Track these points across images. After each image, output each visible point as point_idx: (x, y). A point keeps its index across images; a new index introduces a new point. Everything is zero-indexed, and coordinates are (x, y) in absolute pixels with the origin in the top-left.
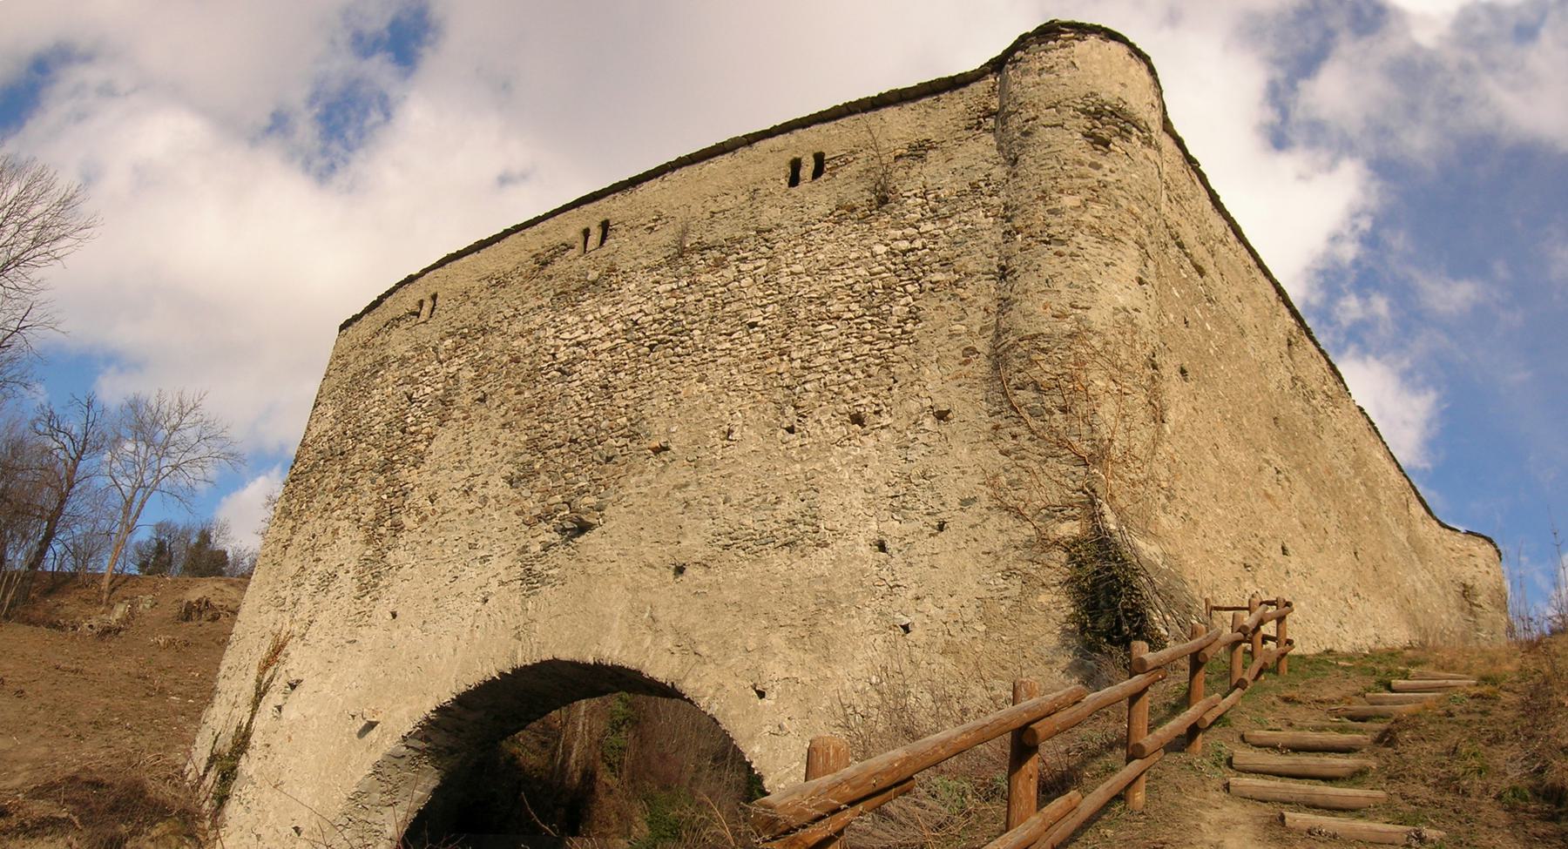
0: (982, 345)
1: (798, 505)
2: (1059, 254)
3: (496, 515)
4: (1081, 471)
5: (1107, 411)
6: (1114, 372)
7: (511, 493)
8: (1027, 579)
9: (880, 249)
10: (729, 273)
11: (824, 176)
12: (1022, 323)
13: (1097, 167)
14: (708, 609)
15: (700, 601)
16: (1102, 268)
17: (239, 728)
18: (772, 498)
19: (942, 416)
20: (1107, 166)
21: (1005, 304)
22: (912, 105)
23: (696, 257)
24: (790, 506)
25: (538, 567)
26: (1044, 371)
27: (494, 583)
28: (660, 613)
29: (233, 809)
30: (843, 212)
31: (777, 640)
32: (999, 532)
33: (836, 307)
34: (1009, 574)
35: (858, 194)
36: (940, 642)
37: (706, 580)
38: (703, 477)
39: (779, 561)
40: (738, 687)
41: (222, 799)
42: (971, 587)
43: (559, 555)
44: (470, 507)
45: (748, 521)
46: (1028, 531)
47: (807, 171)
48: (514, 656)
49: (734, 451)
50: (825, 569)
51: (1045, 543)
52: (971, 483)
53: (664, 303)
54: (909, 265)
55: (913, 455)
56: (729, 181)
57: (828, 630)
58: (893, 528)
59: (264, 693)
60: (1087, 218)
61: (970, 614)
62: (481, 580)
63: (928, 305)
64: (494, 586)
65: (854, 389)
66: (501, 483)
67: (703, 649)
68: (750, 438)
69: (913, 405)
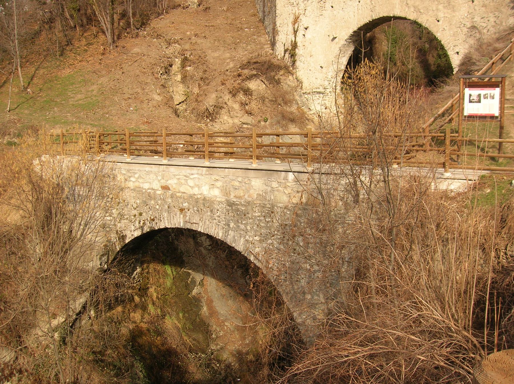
17: (292, 41)
29: (298, 63)
31: (441, 7)
36: (481, 3)
40: (432, 20)
41: (294, 62)
57: (453, 4)
67: (422, 11)
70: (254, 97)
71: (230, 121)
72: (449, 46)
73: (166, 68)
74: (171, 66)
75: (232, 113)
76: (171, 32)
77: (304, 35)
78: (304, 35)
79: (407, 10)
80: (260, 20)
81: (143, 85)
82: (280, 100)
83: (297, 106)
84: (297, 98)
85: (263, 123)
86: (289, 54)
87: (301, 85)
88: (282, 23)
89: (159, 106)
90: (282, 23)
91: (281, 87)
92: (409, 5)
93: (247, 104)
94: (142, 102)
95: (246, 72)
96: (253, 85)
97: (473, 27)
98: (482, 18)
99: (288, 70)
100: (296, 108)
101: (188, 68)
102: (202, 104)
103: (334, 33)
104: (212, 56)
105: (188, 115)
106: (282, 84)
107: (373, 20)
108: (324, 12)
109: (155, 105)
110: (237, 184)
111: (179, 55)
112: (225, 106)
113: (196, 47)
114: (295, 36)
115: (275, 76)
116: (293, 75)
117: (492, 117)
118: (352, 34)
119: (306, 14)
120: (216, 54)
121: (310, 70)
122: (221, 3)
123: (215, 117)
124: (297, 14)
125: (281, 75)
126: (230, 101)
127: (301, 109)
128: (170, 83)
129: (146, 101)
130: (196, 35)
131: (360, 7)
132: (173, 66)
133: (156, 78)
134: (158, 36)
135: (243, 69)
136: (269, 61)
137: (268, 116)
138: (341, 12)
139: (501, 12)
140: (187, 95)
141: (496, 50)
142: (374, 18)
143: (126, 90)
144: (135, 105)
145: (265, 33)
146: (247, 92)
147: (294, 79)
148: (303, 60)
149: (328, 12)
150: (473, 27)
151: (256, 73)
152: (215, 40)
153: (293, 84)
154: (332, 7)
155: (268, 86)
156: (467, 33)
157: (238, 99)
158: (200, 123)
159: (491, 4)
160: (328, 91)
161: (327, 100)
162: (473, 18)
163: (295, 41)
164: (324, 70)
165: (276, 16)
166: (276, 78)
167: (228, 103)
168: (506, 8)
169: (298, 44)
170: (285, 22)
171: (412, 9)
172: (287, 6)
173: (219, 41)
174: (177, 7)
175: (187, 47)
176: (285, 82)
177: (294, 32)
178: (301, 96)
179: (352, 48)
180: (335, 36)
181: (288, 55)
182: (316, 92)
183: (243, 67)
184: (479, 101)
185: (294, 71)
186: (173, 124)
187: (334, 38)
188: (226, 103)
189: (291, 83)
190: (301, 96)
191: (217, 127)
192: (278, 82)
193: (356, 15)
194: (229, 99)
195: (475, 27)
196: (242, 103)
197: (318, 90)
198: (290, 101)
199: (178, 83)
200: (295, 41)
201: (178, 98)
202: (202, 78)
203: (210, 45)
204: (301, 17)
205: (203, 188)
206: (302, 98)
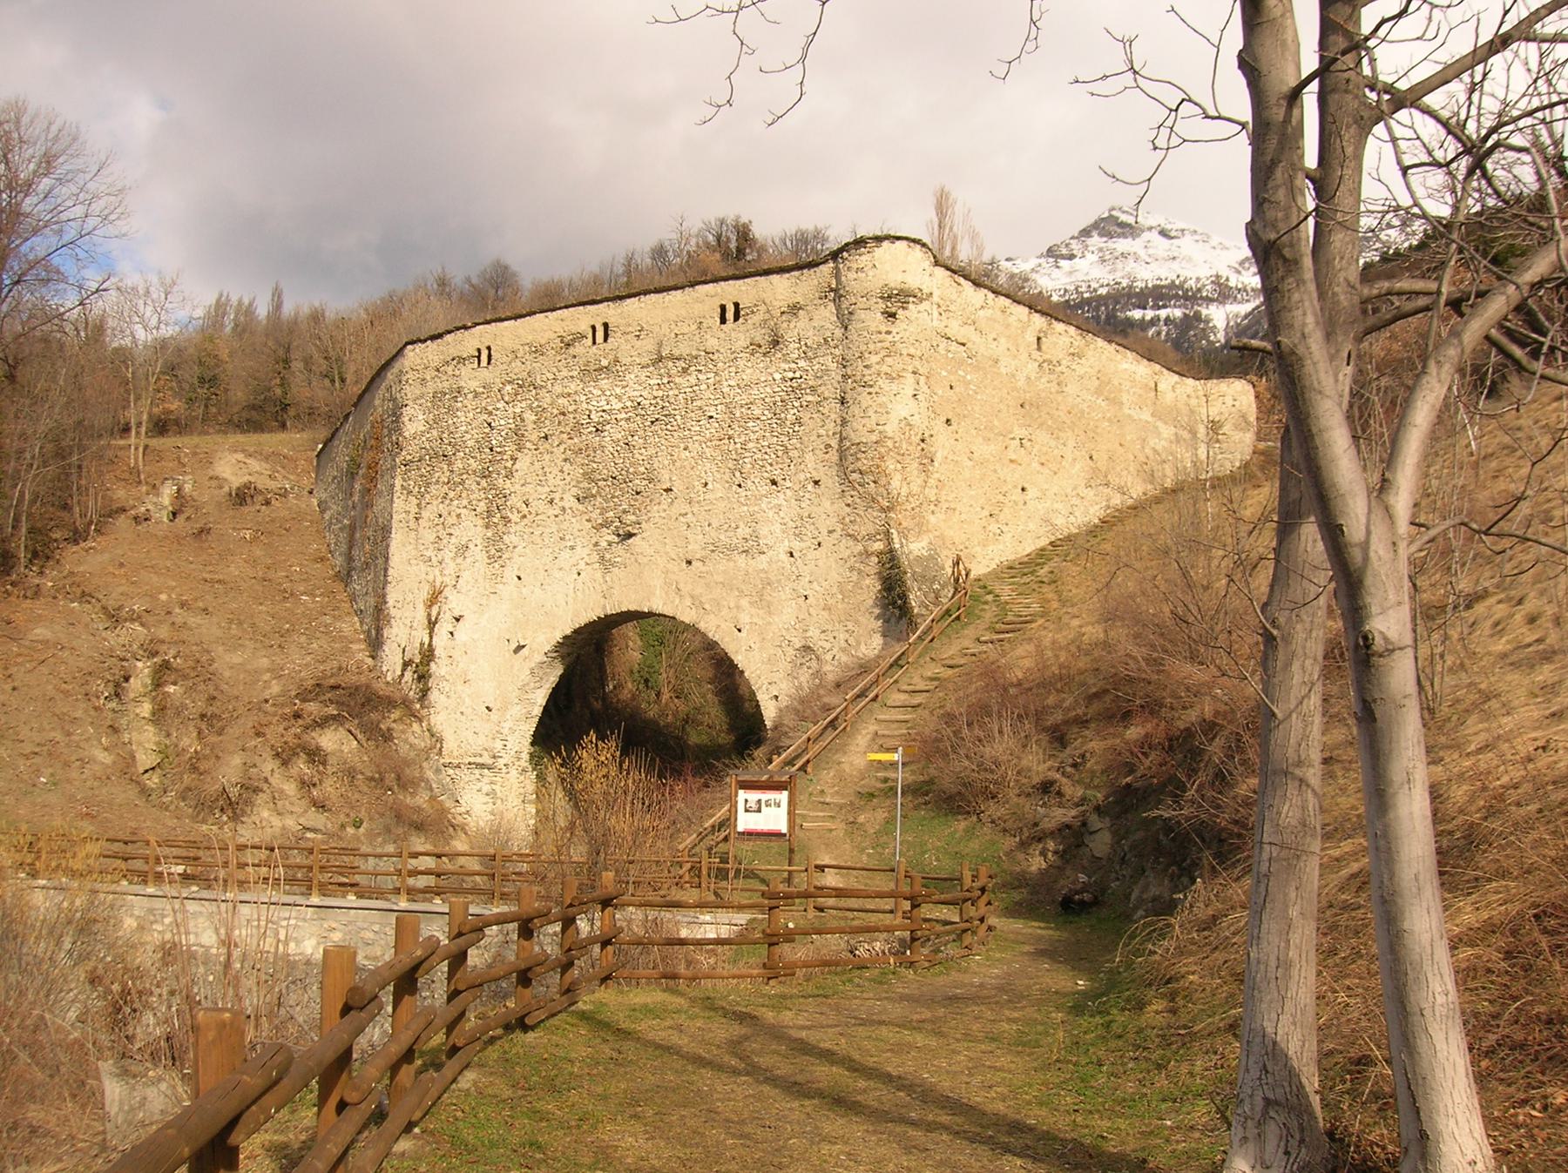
0: (834, 443)
1: (748, 530)
2: (870, 393)
3: (574, 520)
4: (883, 515)
5: (896, 483)
6: (899, 458)
7: (581, 507)
8: (860, 572)
9: (777, 376)
10: (693, 380)
11: (741, 320)
12: (852, 435)
13: (889, 333)
14: (707, 585)
15: (703, 581)
16: (892, 398)
17: (422, 644)
18: (733, 525)
19: (816, 483)
20: (894, 331)
21: (844, 422)
22: (787, 275)
23: (671, 364)
24: (744, 531)
25: (608, 556)
26: (864, 464)
27: (582, 563)
28: (681, 586)
29: (434, 696)
31: (744, 602)
32: (848, 548)
33: (757, 412)
34: (852, 569)
35: (761, 336)
36: (822, 603)
37: (704, 569)
38: (695, 510)
39: (741, 560)
40: (728, 626)
41: (424, 693)
42: (834, 576)
43: (619, 549)
44: (556, 513)
45: (722, 537)
46: (860, 547)
47: (730, 315)
48: (604, 607)
49: (709, 496)
50: (765, 566)
51: (868, 554)
52: (832, 522)
53: (655, 393)
54: (795, 388)
55: (803, 505)
56: (683, 312)
57: (769, 598)
58: (797, 545)
59: (436, 622)
60: (885, 368)
61: (835, 590)
62: (573, 560)
64: (582, 565)
65: (771, 465)
66: (572, 499)
67: (707, 606)
68: (718, 490)
69: (802, 477)
70: (330, 770)
71: (277, 822)
73: (117, 685)
74: (127, 679)
75: (280, 804)
76: (121, 589)
79: (677, 601)
80: (338, 574)
81: (66, 723)
82: (390, 778)
83: (429, 793)
84: (430, 774)
85: (350, 830)
88: (401, 599)
89: (108, 778)
90: (401, 599)
93: (314, 785)
94: (67, 764)
95: (312, 708)
96: (329, 740)
97: (807, 649)
99: (410, 709)
101: (171, 689)
102: (209, 780)
103: (520, 635)
104: (229, 661)
105: (172, 802)
108: (500, 586)
109: (98, 774)
110: (369, 935)
111: (141, 652)
112: (265, 787)
113: (185, 635)
115: (379, 722)
116: (420, 720)
117: (779, 835)
120: (237, 658)
122: (234, 517)
123: (242, 810)
124: (438, 584)
125: (394, 721)
126: (276, 775)
128: (124, 721)
129: (78, 763)
130: (183, 605)
131: (580, 586)
132: (132, 680)
133: (96, 709)
134: (85, 597)
135: (304, 700)
136: (368, 686)
137: (363, 814)
138: (538, 591)
139: (857, 622)
140: (163, 752)
141: (828, 709)
142: (609, 612)
143: (25, 732)
144: (50, 770)
145: (351, 610)
146: (316, 756)
148: (447, 689)
149: (509, 588)
150: (807, 649)
151: (335, 712)
152: (231, 621)
153: (422, 742)
154: (519, 578)
157: (294, 771)
158: (204, 821)
159: (840, 606)
160: (501, 762)
163: (430, 645)
164: (494, 716)
165: (386, 583)
167: (271, 780)
168: (867, 615)
173: (240, 623)
174: (116, 512)
175: (163, 632)
178: (438, 771)
179: (558, 670)
183: (304, 696)
184: (759, 811)
186: (148, 823)
187: (520, 648)
188: (266, 780)
189: (416, 741)
190: (438, 771)
191: (246, 834)
192: (387, 737)
193: (570, 600)
194: (272, 770)
195: (809, 647)
196: (303, 783)
197: (479, 760)
199: (143, 722)
200: (430, 645)
201: (145, 759)
202: (203, 716)
203: (219, 633)
204: (447, 592)
205: (306, 943)
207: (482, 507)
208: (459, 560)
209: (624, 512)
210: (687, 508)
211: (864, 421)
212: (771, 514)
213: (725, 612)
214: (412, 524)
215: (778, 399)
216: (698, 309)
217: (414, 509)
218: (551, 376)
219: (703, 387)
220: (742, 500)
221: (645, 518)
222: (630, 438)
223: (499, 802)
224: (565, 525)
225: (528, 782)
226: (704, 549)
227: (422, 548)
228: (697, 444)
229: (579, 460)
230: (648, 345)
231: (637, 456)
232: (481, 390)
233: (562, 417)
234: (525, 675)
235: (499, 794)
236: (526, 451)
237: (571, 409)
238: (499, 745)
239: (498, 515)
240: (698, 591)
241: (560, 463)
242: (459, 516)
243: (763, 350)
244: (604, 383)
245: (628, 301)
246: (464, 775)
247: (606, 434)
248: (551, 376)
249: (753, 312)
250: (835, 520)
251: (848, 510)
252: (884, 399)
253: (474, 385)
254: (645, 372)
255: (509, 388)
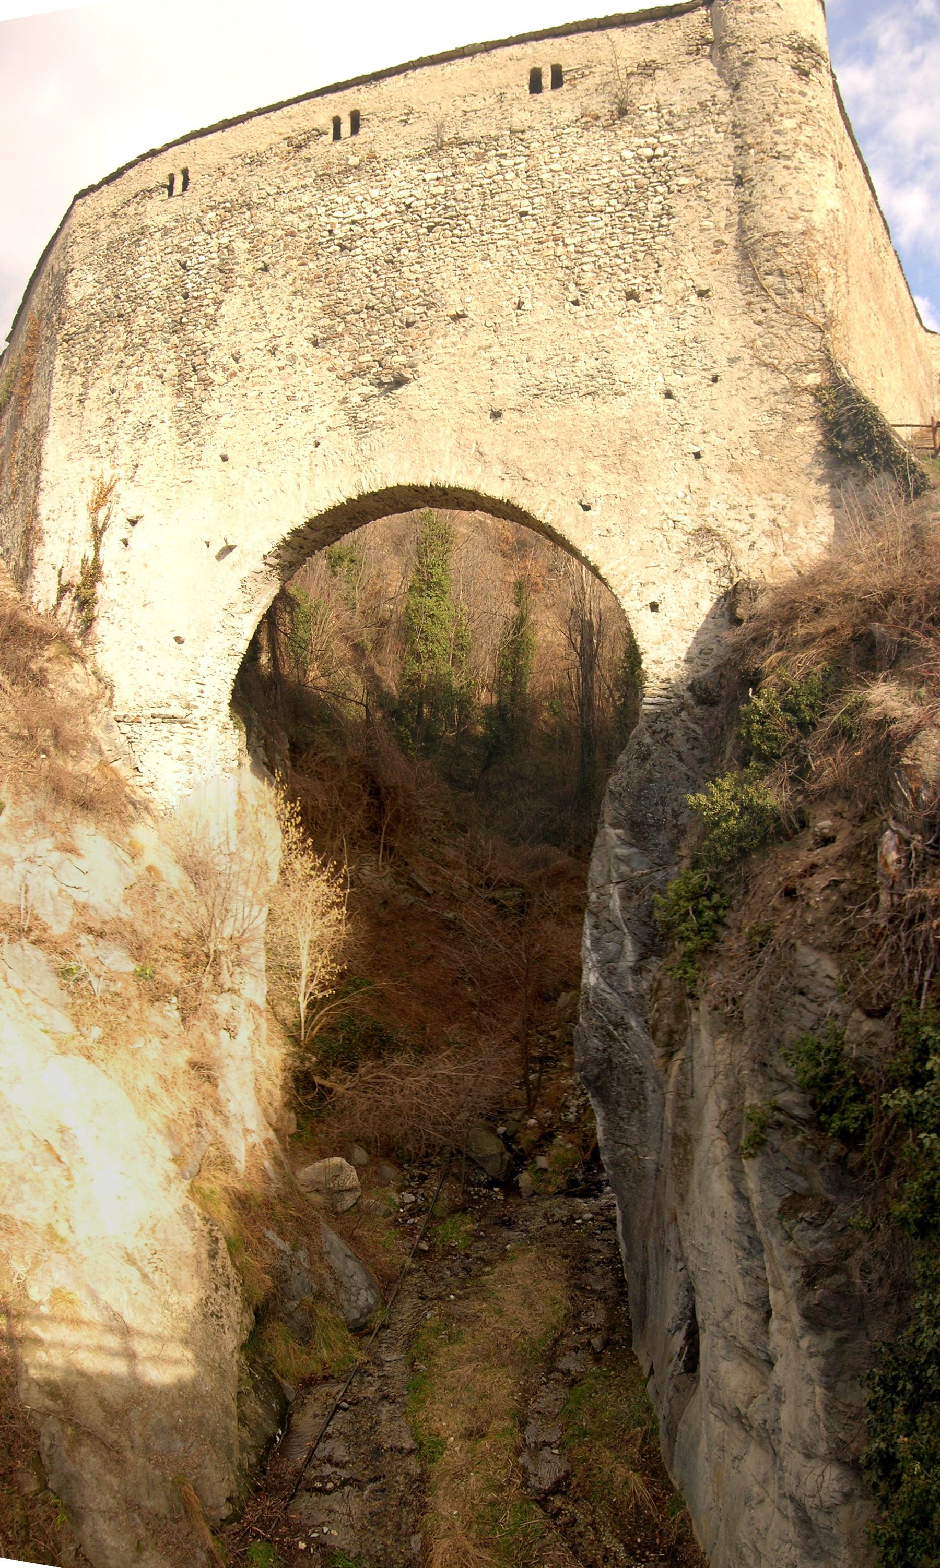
0: (729, 238)
1: (593, 363)
2: (786, 167)
10: (492, 167)
14: (530, 445)
15: (521, 439)
17: (85, 561)
18: (569, 357)
19: (702, 294)
20: (810, 94)
21: (745, 207)
22: (634, 28)
23: (456, 151)
24: (586, 364)
25: (362, 415)
26: (786, 261)
28: (485, 449)
29: (100, 628)
30: (587, 120)
31: (593, 466)
33: (598, 203)
34: (772, 412)
35: (601, 105)
38: (505, 341)
39: (585, 406)
41: (88, 623)
42: (744, 424)
43: (382, 404)
44: (280, 364)
45: (551, 375)
47: (547, 80)
50: (625, 412)
51: (797, 390)
52: (735, 346)
56: (475, 83)
58: (676, 381)
61: (746, 443)
63: (678, 204)
65: (627, 271)
66: (306, 344)
67: (530, 475)
68: (540, 309)
69: (679, 285)
72: (626, 583)
77: (126, 543)
78: (126, 543)
82: (44, 736)
83: (97, 757)
84: (97, 731)
86: (75, 599)
87: (108, 694)
91: (49, 695)
92: (487, 459)
97: (705, 533)
98: (734, 507)
99: (70, 647)
100: (96, 764)
106: (51, 686)
107: (359, 496)
108: (198, 472)
114: (96, 544)
116: (83, 661)
118: (288, 538)
119: (136, 478)
121: (141, 648)
124: (107, 480)
127: (112, 770)
136: (14, 615)
142: (367, 490)
147: (87, 674)
153: (89, 688)
155: (9, 689)
156: (684, 546)
161: (196, 744)
162: (704, 506)
163: (96, 560)
165: (38, 489)
166: (33, 667)
168: (804, 478)
169: (105, 570)
170: (66, 506)
171: (498, 470)
172: (78, 455)
176: (61, 679)
177: (95, 531)
178: (108, 728)
180: (231, 543)
181: (70, 601)
182: (159, 716)
185: (88, 651)
190: (108, 728)
192: (40, 680)
197: (165, 711)
198: (75, 742)
200: (96, 560)
204: (120, 488)
206: (112, 735)
207: (172, 370)
208: (138, 444)
209: (388, 352)
210: (490, 338)
211: (781, 204)
212: (630, 338)
213: (560, 482)
214: (75, 409)
215: (630, 184)
216: (496, 78)
217: (77, 390)
218: (271, 190)
219: (510, 176)
220: (583, 321)
221: (422, 356)
222: (394, 252)
223: (196, 769)
224: (294, 380)
225: (229, 743)
226: (521, 393)
227: (87, 436)
228: (503, 252)
229: (316, 290)
230: (422, 129)
231: (407, 275)
232: (173, 224)
233: (290, 239)
234: (232, 591)
235: (196, 760)
236: (235, 289)
237: (303, 226)
238: (194, 689)
239: (195, 378)
240: (515, 453)
241: (286, 297)
242: (139, 386)
243: (602, 122)
244: (353, 187)
245: (389, 80)
246: (146, 732)
247: (358, 251)
248: (271, 190)
249: (583, 76)
250: (740, 343)
251: (759, 329)
252: (806, 177)
253: (161, 220)
254: (417, 165)
255: (212, 215)
